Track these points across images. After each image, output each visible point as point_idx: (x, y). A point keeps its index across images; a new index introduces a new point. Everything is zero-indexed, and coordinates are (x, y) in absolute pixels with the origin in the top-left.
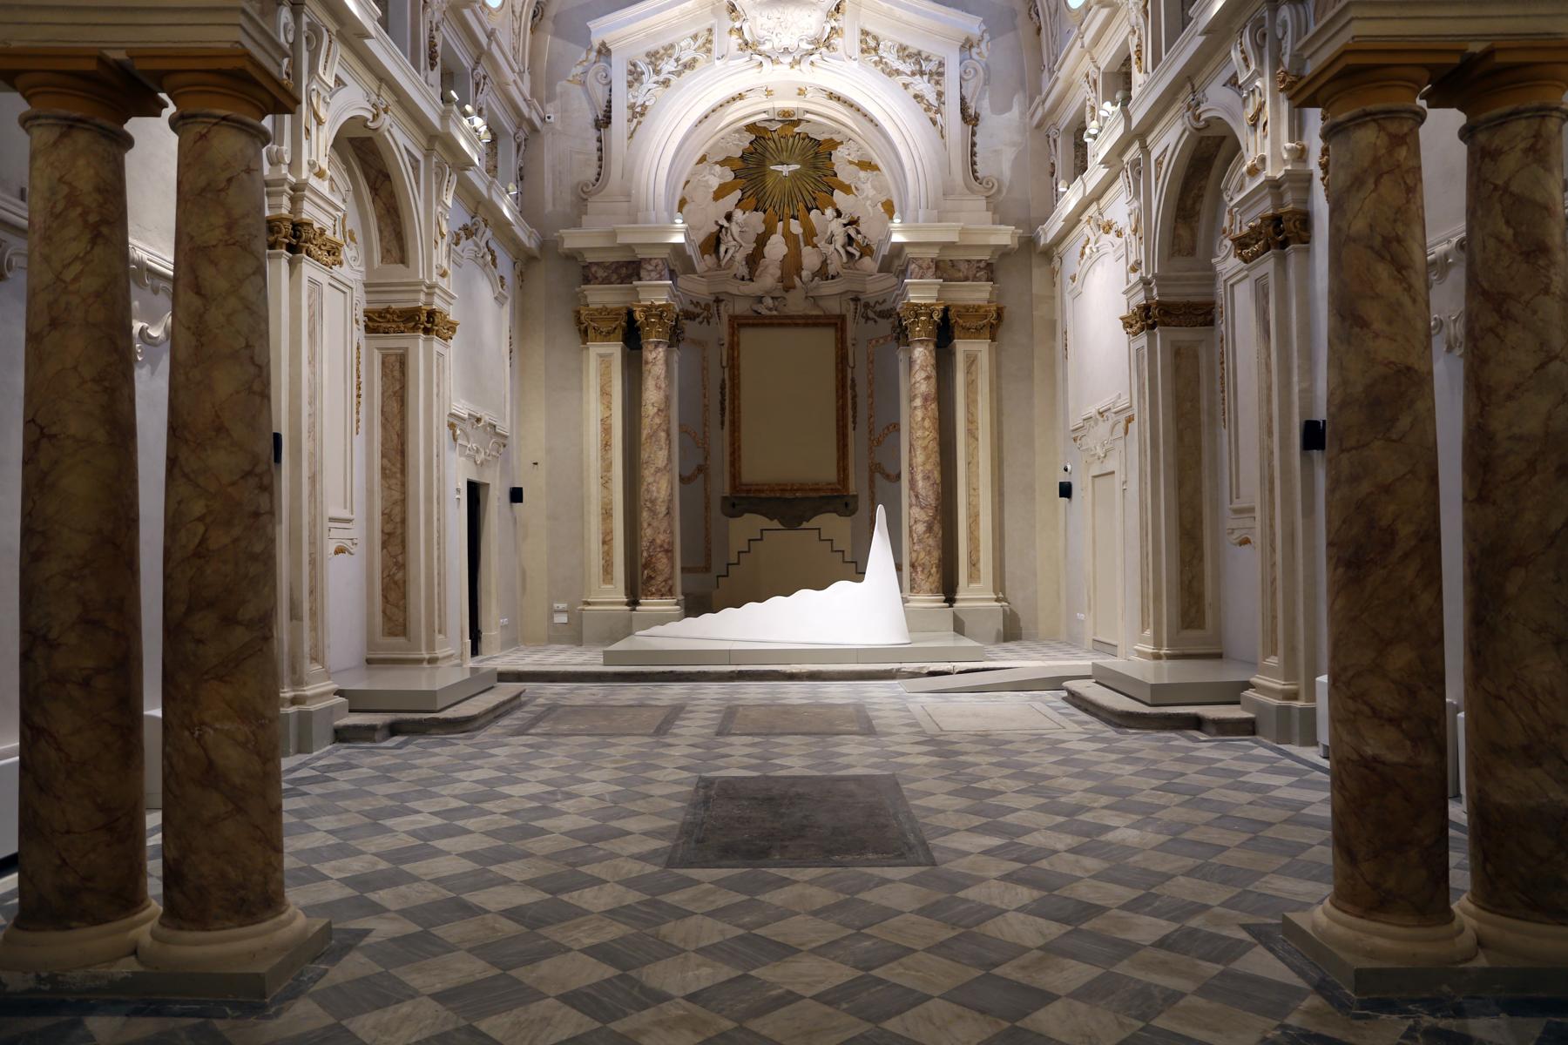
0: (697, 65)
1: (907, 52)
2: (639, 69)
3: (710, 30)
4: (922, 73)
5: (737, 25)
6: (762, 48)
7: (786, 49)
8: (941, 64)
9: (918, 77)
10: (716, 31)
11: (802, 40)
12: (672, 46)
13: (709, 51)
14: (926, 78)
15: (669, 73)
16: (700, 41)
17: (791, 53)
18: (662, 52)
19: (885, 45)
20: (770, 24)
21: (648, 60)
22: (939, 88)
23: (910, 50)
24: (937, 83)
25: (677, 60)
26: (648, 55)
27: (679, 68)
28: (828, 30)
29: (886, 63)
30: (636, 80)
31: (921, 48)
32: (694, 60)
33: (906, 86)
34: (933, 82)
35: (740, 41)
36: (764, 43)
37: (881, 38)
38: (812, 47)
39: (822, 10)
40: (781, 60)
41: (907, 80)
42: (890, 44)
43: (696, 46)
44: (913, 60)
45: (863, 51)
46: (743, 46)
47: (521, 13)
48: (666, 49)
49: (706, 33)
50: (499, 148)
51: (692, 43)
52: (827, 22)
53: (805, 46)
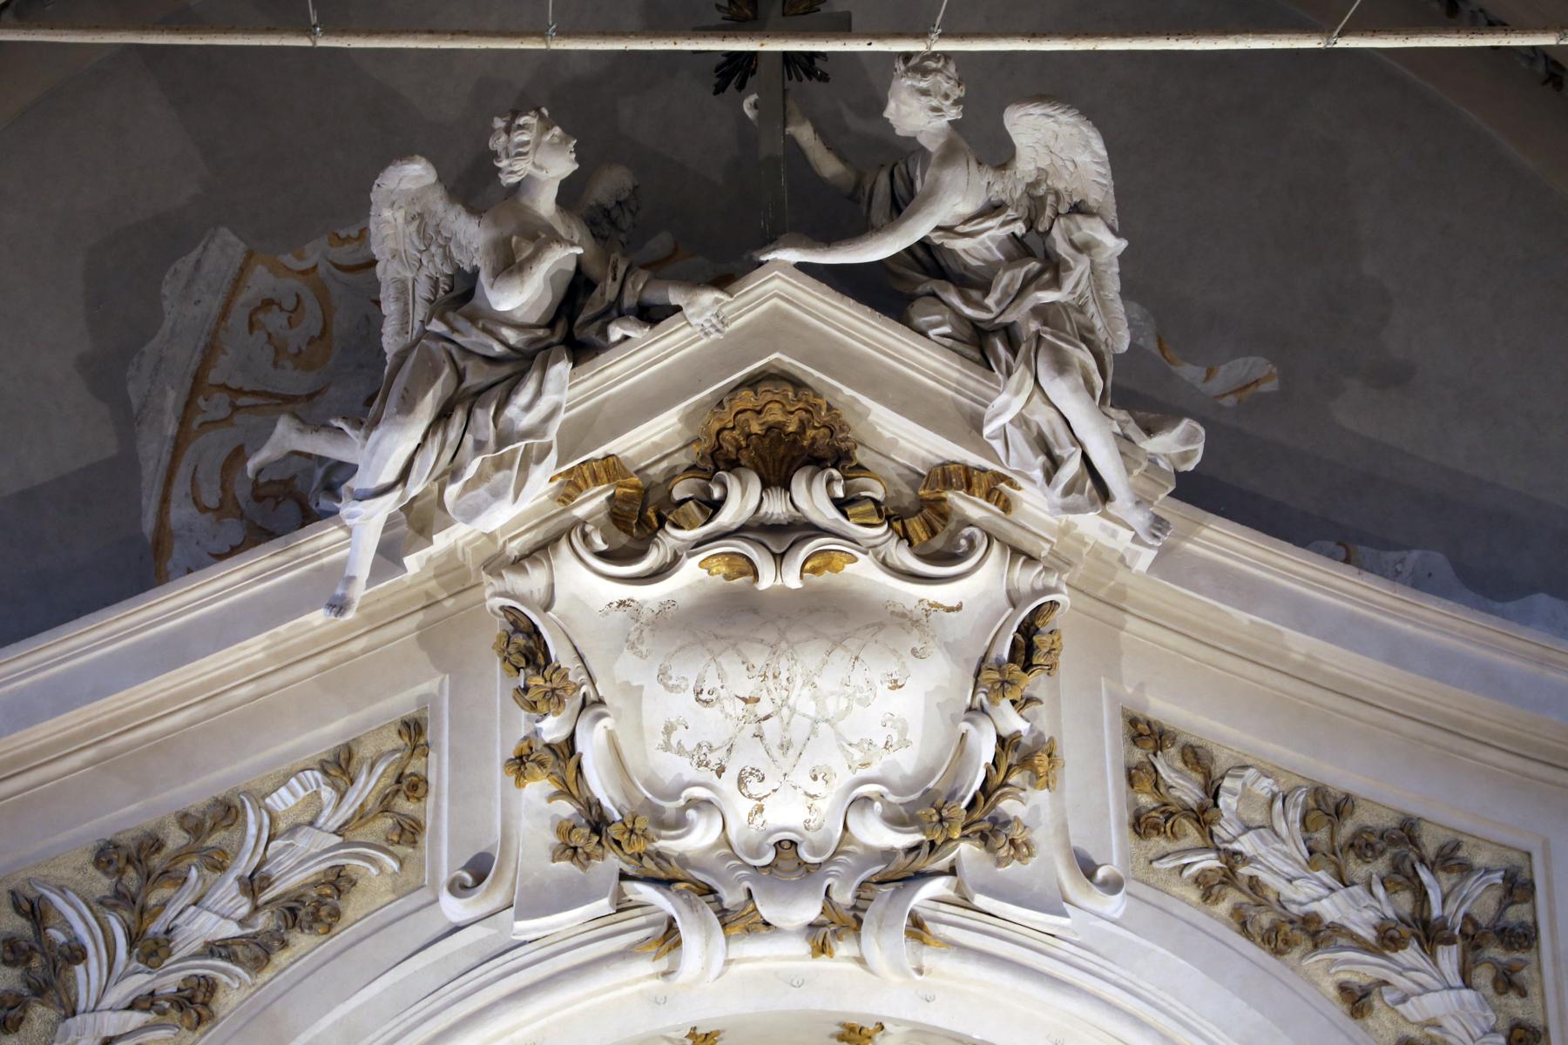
0: (353, 906)
1: (1347, 829)
2: (58, 936)
3: (413, 730)
4: (1429, 934)
5: (552, 728)
6: (672, 845)
7: (785, 848)
8: (1517, 887)
9: (1410, 955)
10: (442, 735)
11: (866, 800)
12: (227, 812)
13: (410, 831)
14: (1449, 957)
15: (214, 949)
16: (367, 786)
17: (807, 869)
18: (176, 838)
19: (1246, 796)
20: (712, 725)
21: (102, 885)
22: (1516, 1007)
23: (1363, 817)
24: (1507, 981)
25: (253, 885)
26: (106, 856)
27: (263, 921)
28: (986, 750)
29: (1254, 885)
30: (40, 990)
31: (1414, 808)
32: (338, 881)
33: (1357, 1000)
34: (1484, 976)
35: (566, 809)
36: (679, 823)
37: (1223, 760)
38: (901, 840)
39: (950, 648)
40: (767, 911)
41: (1362, 968)
42: (1265, 787)
43: (346, 811)
44: (1381, 866)
45: (1141, 825)
46: (581, 837)
48: (194, 825)
49: (394, 741)
51: (327, 794)
52: (976, 711)
53: (877, 834)
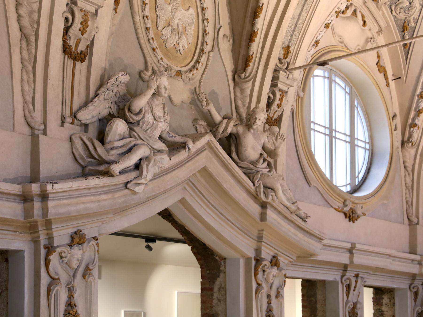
47: (414, 166)
50: (397, 300)
